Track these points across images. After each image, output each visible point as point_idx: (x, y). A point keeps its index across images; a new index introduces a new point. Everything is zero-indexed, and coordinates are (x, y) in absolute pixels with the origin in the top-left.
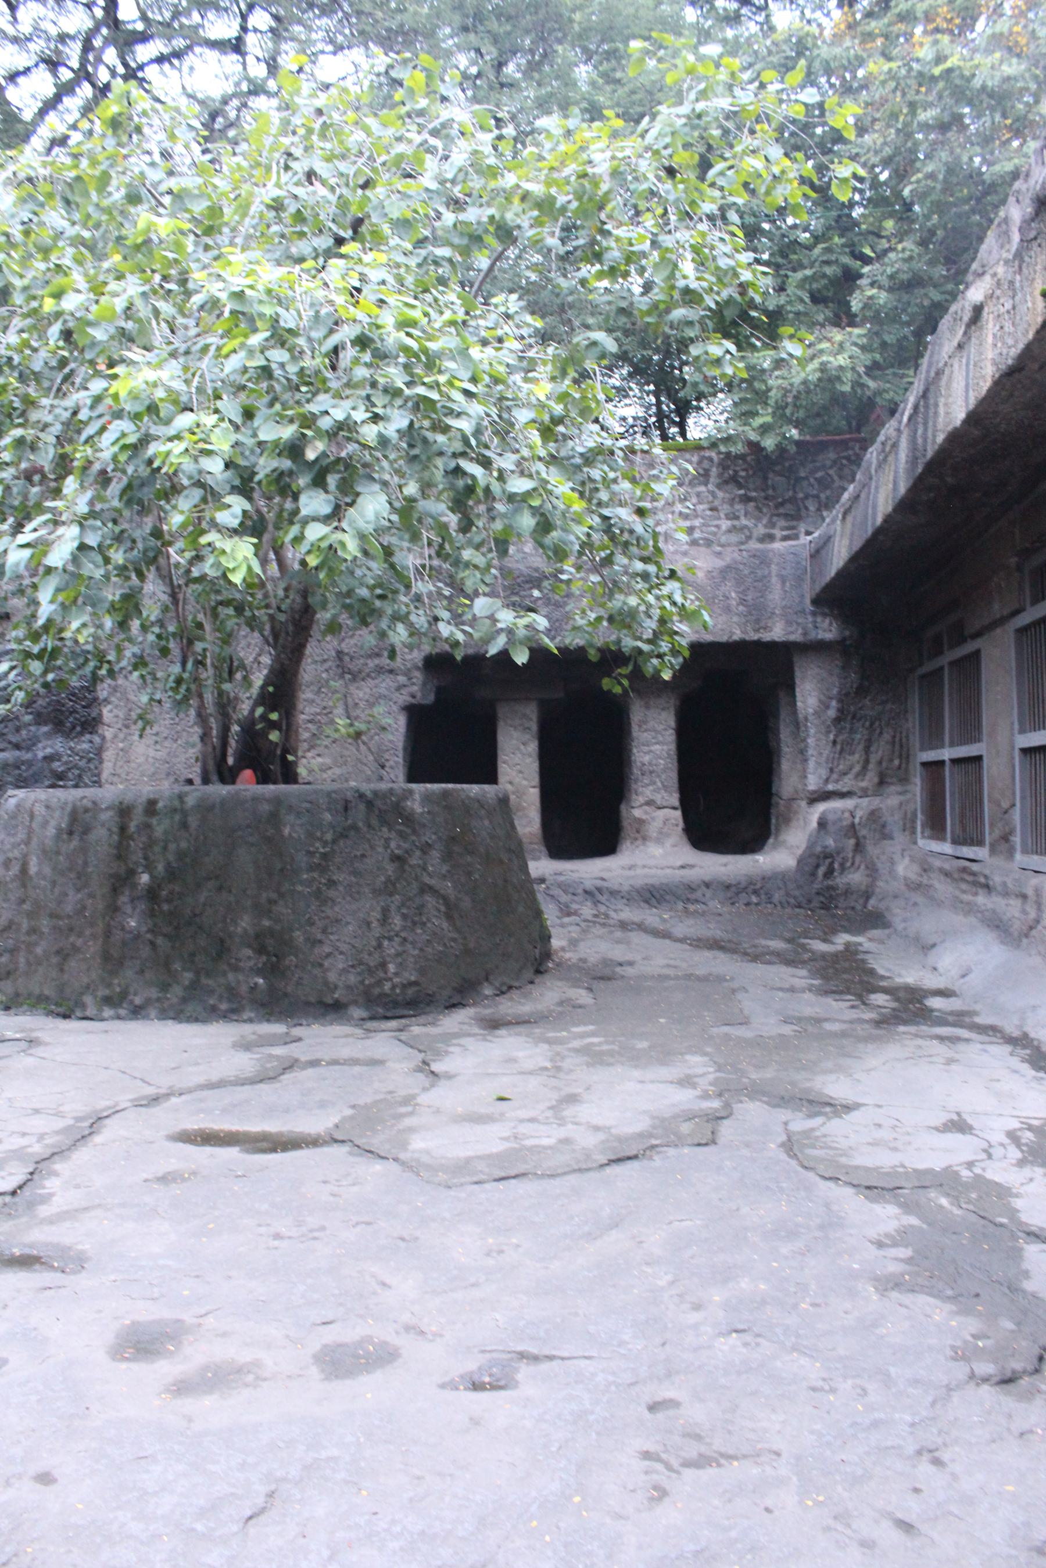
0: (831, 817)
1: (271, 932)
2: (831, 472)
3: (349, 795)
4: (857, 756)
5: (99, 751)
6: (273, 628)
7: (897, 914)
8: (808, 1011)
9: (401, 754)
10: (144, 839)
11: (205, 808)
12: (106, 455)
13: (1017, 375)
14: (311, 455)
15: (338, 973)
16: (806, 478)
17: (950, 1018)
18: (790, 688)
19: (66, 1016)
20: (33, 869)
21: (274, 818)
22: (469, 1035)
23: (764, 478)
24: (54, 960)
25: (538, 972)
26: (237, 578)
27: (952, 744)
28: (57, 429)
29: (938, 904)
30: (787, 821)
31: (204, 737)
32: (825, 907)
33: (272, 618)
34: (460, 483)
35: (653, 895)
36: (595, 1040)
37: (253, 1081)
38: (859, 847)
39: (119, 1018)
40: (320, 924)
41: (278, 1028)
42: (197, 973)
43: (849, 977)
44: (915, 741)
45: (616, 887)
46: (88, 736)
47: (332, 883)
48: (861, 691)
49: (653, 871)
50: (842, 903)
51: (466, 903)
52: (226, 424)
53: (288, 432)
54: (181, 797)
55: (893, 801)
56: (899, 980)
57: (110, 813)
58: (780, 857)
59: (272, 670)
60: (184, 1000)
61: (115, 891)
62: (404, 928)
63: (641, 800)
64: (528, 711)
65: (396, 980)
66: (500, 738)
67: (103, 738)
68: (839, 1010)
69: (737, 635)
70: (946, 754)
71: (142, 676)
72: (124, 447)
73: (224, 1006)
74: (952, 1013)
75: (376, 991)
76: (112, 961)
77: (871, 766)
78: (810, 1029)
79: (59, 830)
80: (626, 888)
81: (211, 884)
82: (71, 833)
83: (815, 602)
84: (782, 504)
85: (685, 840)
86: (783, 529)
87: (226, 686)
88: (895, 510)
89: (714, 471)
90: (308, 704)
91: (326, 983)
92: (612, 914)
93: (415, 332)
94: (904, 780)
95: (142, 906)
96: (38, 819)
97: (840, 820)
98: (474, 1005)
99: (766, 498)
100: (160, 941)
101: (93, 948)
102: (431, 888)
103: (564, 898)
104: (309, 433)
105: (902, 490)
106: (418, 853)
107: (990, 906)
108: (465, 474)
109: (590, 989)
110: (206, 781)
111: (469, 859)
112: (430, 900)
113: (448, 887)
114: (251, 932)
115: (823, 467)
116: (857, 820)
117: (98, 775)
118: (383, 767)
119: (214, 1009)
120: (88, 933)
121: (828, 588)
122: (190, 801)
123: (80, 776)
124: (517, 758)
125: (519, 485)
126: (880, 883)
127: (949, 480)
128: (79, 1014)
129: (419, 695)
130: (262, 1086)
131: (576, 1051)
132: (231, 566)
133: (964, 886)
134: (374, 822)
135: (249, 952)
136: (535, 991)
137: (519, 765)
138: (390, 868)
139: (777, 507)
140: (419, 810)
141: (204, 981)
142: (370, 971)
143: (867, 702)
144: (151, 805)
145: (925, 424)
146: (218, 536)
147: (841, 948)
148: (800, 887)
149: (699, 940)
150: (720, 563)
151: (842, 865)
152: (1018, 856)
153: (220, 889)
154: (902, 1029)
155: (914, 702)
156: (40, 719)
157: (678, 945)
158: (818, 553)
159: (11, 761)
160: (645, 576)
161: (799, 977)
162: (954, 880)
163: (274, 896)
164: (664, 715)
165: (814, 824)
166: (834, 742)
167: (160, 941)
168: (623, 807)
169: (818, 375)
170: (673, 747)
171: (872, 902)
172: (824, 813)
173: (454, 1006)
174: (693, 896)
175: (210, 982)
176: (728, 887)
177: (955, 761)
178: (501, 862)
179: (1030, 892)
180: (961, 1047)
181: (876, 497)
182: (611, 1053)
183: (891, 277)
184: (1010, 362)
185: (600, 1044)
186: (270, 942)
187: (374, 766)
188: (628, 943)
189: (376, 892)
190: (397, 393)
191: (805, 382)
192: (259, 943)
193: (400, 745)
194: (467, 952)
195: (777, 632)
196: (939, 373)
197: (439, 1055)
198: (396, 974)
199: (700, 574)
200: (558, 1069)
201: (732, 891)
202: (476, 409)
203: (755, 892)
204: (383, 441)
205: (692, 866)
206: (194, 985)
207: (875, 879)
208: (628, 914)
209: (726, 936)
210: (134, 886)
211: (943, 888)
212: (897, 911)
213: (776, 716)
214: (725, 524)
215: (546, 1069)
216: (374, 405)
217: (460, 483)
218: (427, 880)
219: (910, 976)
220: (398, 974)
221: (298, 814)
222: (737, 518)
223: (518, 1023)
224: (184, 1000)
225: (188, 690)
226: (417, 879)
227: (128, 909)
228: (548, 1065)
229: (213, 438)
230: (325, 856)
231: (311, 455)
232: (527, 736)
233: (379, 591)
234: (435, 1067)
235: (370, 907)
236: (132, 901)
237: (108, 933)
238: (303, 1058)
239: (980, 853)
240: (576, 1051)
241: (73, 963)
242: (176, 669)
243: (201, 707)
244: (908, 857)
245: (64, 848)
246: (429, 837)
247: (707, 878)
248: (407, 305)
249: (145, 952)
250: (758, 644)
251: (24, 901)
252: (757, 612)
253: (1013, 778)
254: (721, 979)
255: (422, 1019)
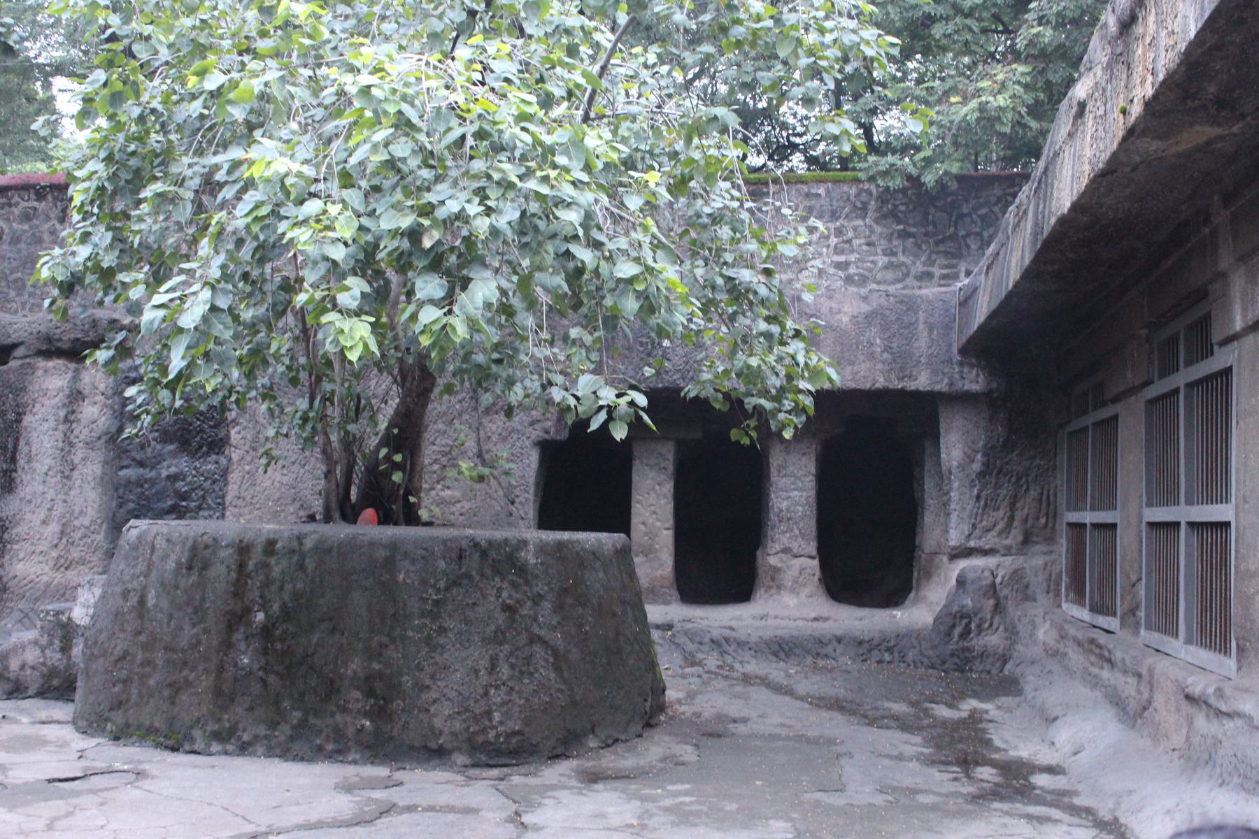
0: (971, 576)
1: (380, 674)
2: (996, 209)
3: (464, 544)
4: (1001, 513)
5: (225, 473)
6: (401, 370)
7: (1030, 681)
8: (908, 781)
9: (532, 490)
10: (261, 577)
11: (323, 550)
12: (241, 223)
13: (1109, 177)
14: (427, 243)
15: (444, 719)
16: (969, 214)
17: (1049, 797)
18: (936, 437)
19: (174, 749)
20: (151, 602)
21: (389, 564)
22: (565, 788)
23: (934, 210)
24: (166, 693)
25: (648, 725)
26: (353, 356)
27: (1093, 509)
28: (195, 183)
29: (1070, 673)
30: (929, 576)
31: (328, 474)
32: (961, 670)
33: (400, 360)
34: (571, 265)
35: (782, 648)
36: (688, 799)
37: (349, 824)
38: (998, 608)
39: (226, 753)
40: (429, 670)
41: (381, 771)
42: (306, 713)
43: (963, 748)
44: (1062, 499)
45: (743, 638)
46: (214, 457)
47: (443, 630)
48: (1008, 446)
49: (785, 623)
50: (977, 665)
51: (575, 655)
52: (349, 213)
53: (406, 222)
54: (300, 538)
55: (1038, 561)
56: (1012, 753)
57: (230, 551)
58: (918, 614)
59: (397, 412)
60: (292, 739)
61: (230, 628)
62: (511, 678)
63: (777, 547)
64: (664, 451)
65: (501, 729)
66: (635, 478)
67: (230, 460)
68: (942, 780)
69: (881, 383)
70: (1088, 517)
71: (270, 409)
72: (256, 219)
73: (330, 747)
74: (1052, 792)
75: (481, 739)
76: (223, 697)
77: (1016, 523)
78: (902, 800)
79: (179, 564)
80: (754, 639)
81: (324, 626)
82: (190, 568)
83: (963, 351)
84: (942, 241)
85: (821, 591)
86: (942, 267)
87: (352, 427)
88: (1021, 277)
89: (872, 204)
90: (435, 441)
91: (432, 728)
92: (737, 666)
93: (531, 127)
94: (1051, 540)
95: (256, 644)
96: (159, 553)
97: (979, 579)
98: (578, 756)
99: (926, 234)
100: (272, 679)
101: (206, 683)
102: (540, 638)
103: (690, 647)
104: (426, 222)
105: (1027, 262)
106: (529, 603)
107: (1113, 682)
108: (574, 257)
109: (697, 746)
110: (328, 519)
111: (580, 611)
112: (539, 650)
113: (558, 639)
114: (361, 675)
115: (987, 204)
116: (998, 580)
117: (223, 497)
118: (513, 503)
119: (320, 749)
120: (201, 668)
121: (971, 340)
122: (308, 543)
123: (204, 497)
124: (652, 499)
125: (626, 269)
126: (1019, 647)
127: (1071, 256)
128: (187, 748)
129: (553, 430)
130: (357, 828)
131: (666, 809)
132: (348, 345)
133: (1093, 658)
134: (488, 572)
135: (357, 694)
136: (641, 745)
137: (653, 504)
138: (501, 618)
139: (937, 243)
140: (533, 561)
141: (312, 720)
142: (476, 719)
143: (1014, 456)
144: (270, 545)
145: (1045, 201)
146: (338, 316)
147: (965, 714)
148: (934, 647)
149: (821, 698)
150: (865, 308)
151: (979, 626)
152: (1143, 632)
153: (333, 630)
154: (996, 805)
155: (1063, 460)
156: (166, 437)
157: (799, 703)
158: (966, 301)
159: (134, 478)
160: (768, 336)
161: (912, 744)
162: (1085, 651)
163: (385, 640)
164: (804, 460)
165: (954, 582)
166: (978, 497)
167: (272, 679)
168: (759, 553)
169: (976, 115)
170: (813, 493)
171: (1009, 666)
172: (963, 570)
173: (558, 756)
174: (823, 651)
175: (319, 722)
176: (861, 643)
177: (1096, 526)
178: (614, 615)
179: (1144, 672)
180: (1048, 827)
181: (1010, 261)
182: (698, 814)
183: (1058, 14)
184: (1101, 165)
185: (691, 803)
186: (378, 685)
187: (504, 501)
188: (747, 699)
189: (486, 641)
190: (511, 186)
191: (964, 120)
192: (368, 686)
193: (532, 480)
194: (574, 703)
195: (922, 381)
196: (1056, 154)
197: (532, 806)
198: (501, 723)
199: (845, 319)
200: (643, 827)
201: (865, 647)
202: (587, 197)
203: (888, 650)
204: (495, 232)
205: (826, 619)
206: (302, 724)
207: (1014, 643)
208: (753, 667)
209: (850, 696)
210: (249, 624)
211: (1076, 658)
212: (1031, 678)
213: (922, 467)
214: (882, 260)
215: (631, 826)
216: (487, 198)
217: (571, 265)
218: (536, 630)
219: (1024, 750)
220: (503, 723)
221: (413, 562)
222: (894, 254)
223: (617, 778)
224: (292, 739)
225: (313, 428)
226: (526, 629)
227: (242, 646)
228: (635, 822)
229: (337, 225)
230: (437, 603)
231: (427, 243)
232: (662, 477)
233: (495, 356)
234: (526, 819)
235: (478, 656)
236: (247, 638)
237: (221, 669)
238: (401, 804)
239: (1112, 623)
240: (666, 809)
241: (184, 697)
242: (303, 404)
243: (328, 442)
244: (1050, 622)
245: (183, 583)
246: (541, 588)
247: (839, 633)
248: (523, 101)
249: (256, 688)
250: (902, 392)
251: (140, 633)
252: (902, 361)
253: (1141, 551)
254: (831, 742)
255: (523, 769)
